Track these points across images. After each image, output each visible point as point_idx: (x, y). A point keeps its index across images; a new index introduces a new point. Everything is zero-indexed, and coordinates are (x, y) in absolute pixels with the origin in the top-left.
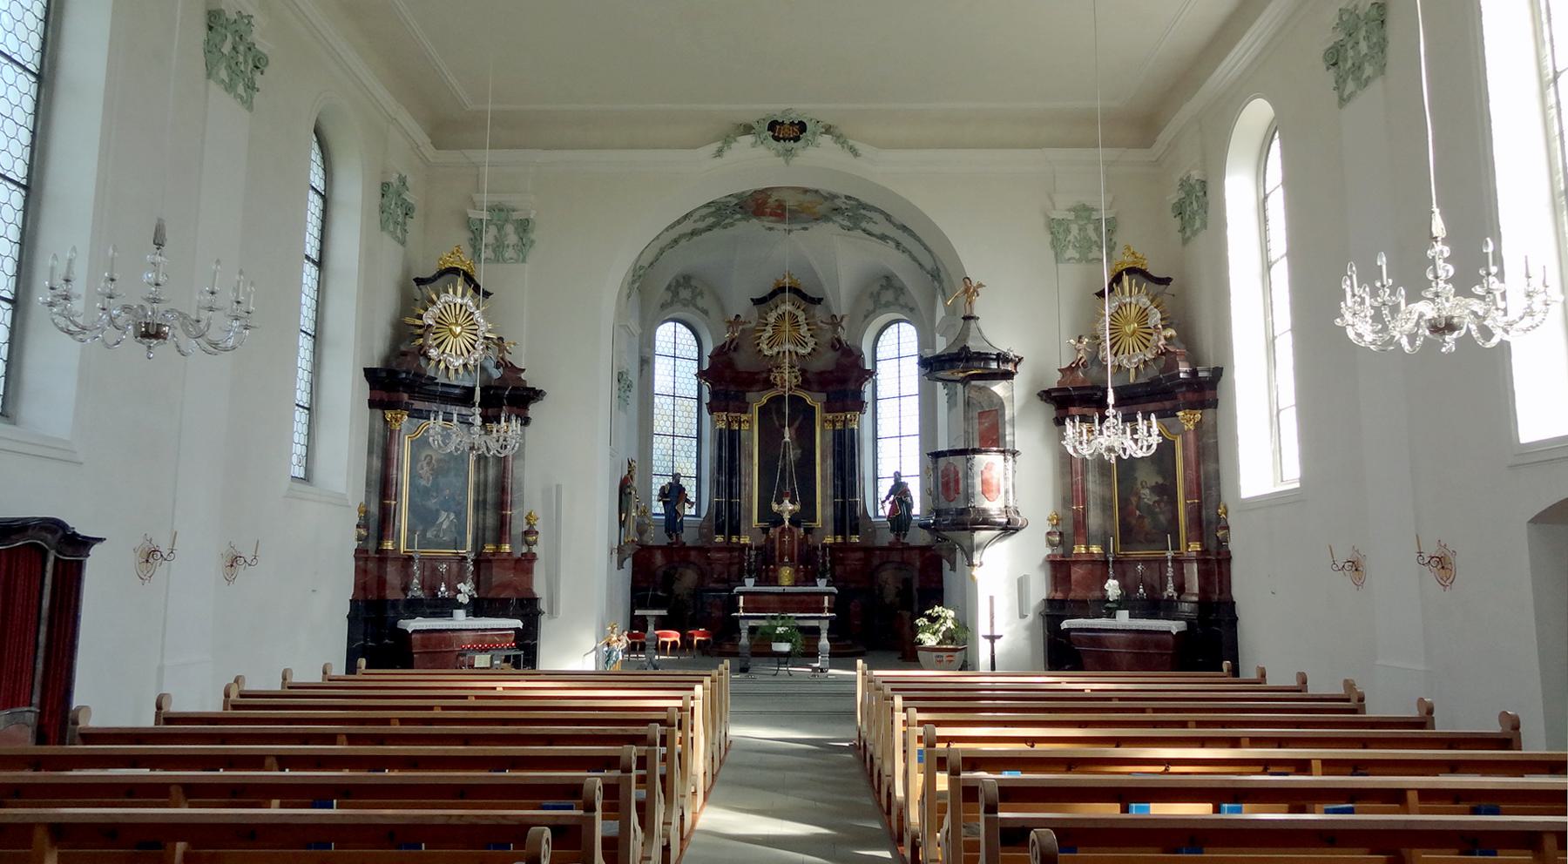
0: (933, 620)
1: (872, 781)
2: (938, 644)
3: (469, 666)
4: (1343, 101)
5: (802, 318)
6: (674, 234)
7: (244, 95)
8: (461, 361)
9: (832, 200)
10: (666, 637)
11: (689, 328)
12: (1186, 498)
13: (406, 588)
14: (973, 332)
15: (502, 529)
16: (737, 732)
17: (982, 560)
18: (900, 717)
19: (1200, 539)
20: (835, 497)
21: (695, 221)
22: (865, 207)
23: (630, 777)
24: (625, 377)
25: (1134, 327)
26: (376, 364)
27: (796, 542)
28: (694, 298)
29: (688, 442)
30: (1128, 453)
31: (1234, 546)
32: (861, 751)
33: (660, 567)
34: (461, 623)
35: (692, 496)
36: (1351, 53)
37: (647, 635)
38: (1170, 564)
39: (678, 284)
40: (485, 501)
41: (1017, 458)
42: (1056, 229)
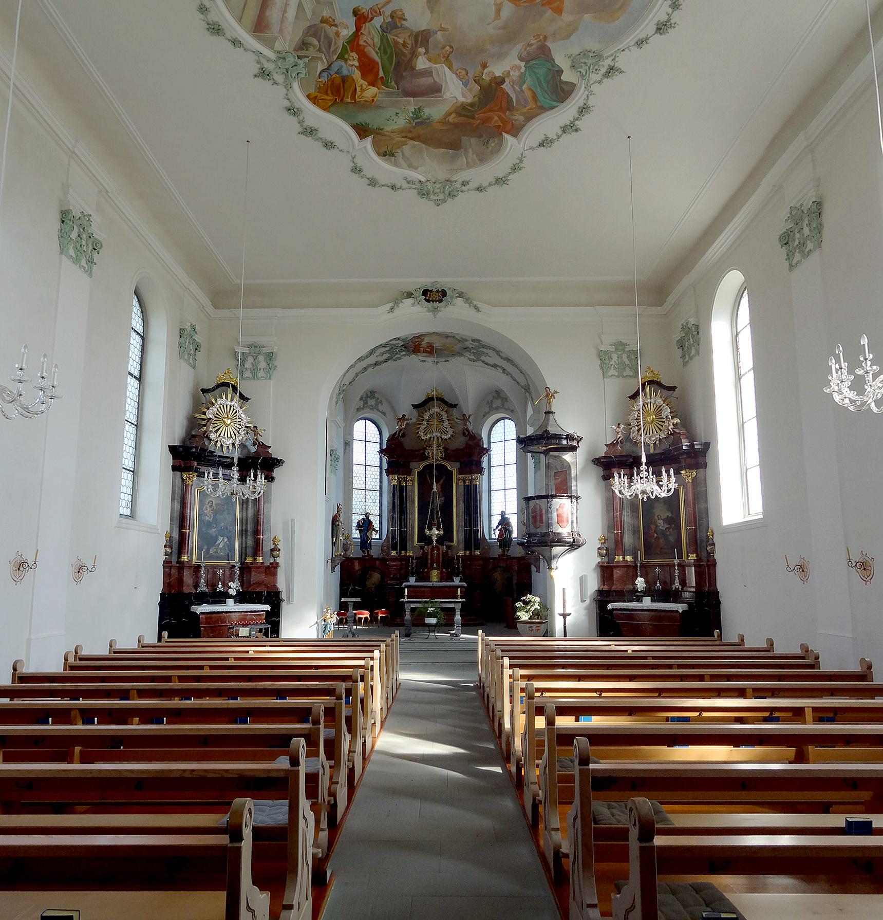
0: (526, 603)
1: (484, 700)
2: (529, 619)
3: (235, 635)
4: (792, 267)
5: (445, 416)
6: (364, 364)
7: (86, 266)
8: (231, 442)
9: (463, 342)
10: (361, 615)
11: (374, 423)
12: (686, 526)
13: (196, 586)
14: (551, 421)
15: (257, 549)
16: (405, 676)
17: (557, 565)
18: (507, 672)
19: (696, 552)
20: (465, 526)
21: (377, 356)
22: (484, 347)
23: (319, 728)
24: (334, 452)
25: (653, 418)
26: (177, 443)
27: (441, 555)
28: (377, 404)
29: (374, 493)
30: (654, 495)
31: (718, 556)
32: (480, 689)
33: (357, 571)
34: (232, 607)
35: (377, 526)
36: (797, 235)
37: (348, 614)
38: (676, 568)
39: (367, 396)
40: (246, 531)
41: (579, 501)
42: (604, 357)
